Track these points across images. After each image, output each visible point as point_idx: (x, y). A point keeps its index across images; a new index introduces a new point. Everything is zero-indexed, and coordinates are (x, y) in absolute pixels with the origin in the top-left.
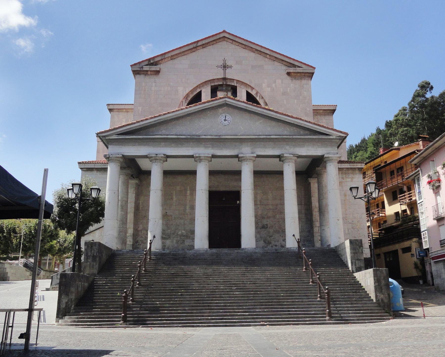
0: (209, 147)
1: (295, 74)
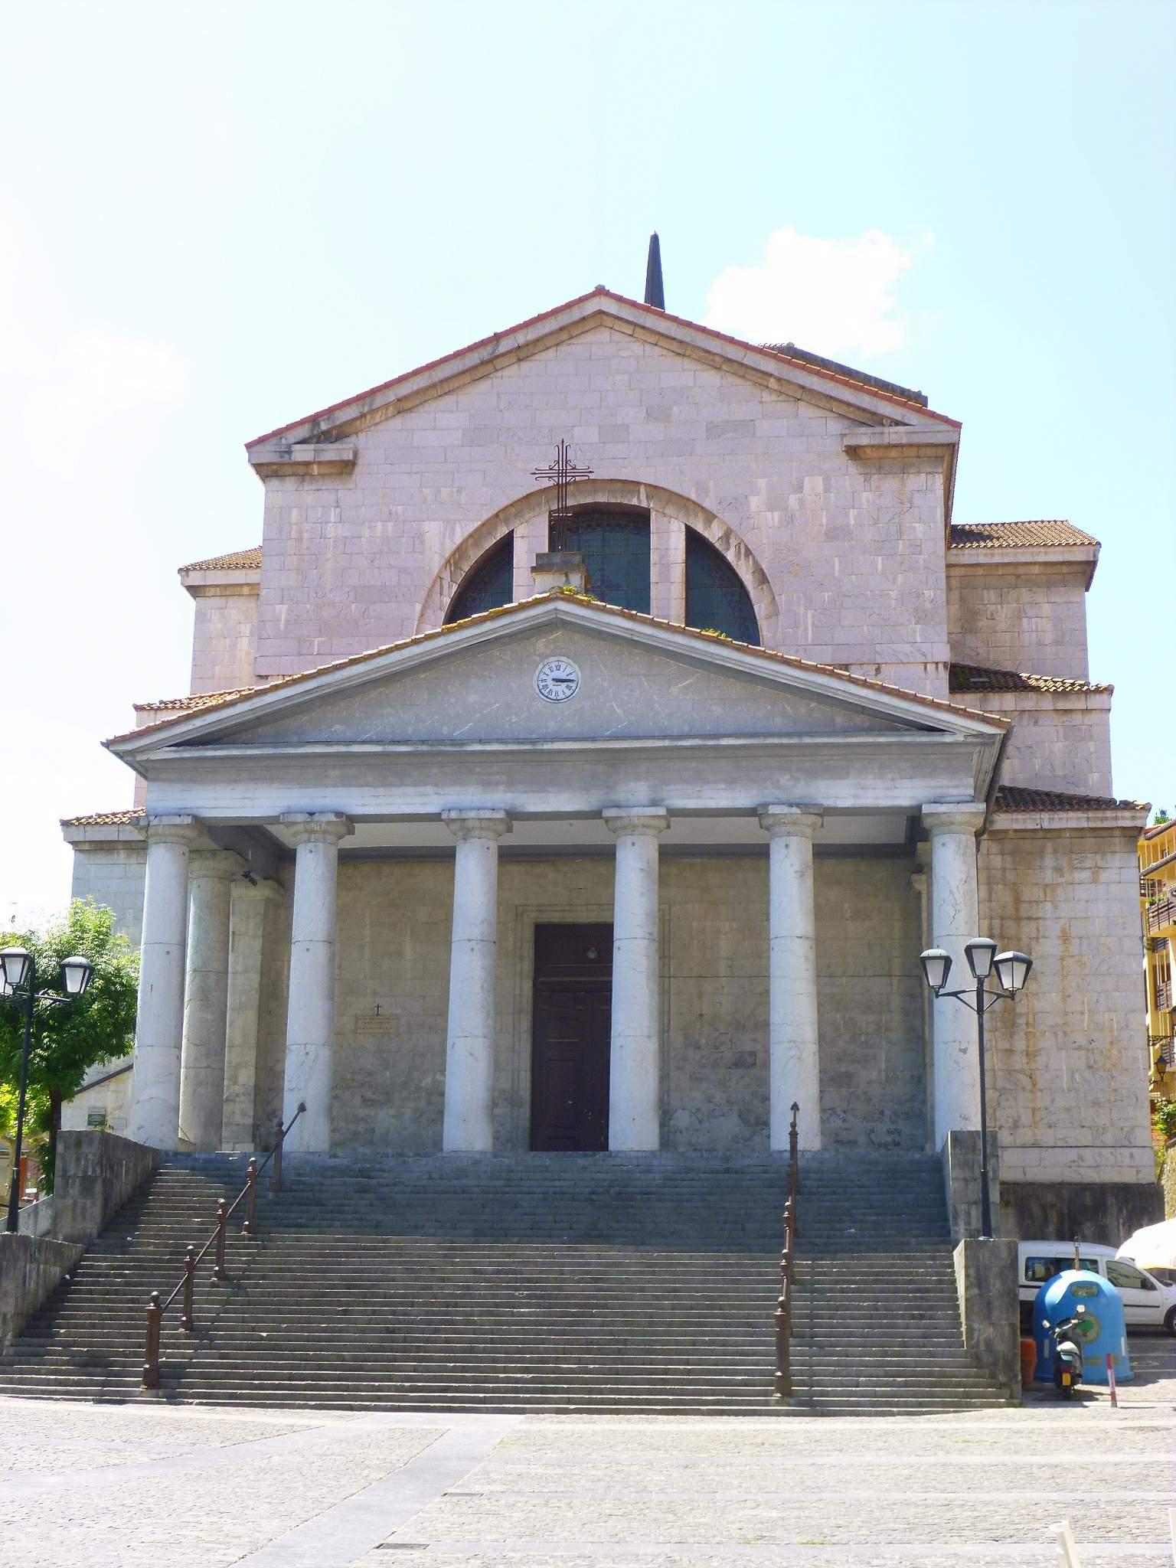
0: (497, 783)
1: (880, 453)
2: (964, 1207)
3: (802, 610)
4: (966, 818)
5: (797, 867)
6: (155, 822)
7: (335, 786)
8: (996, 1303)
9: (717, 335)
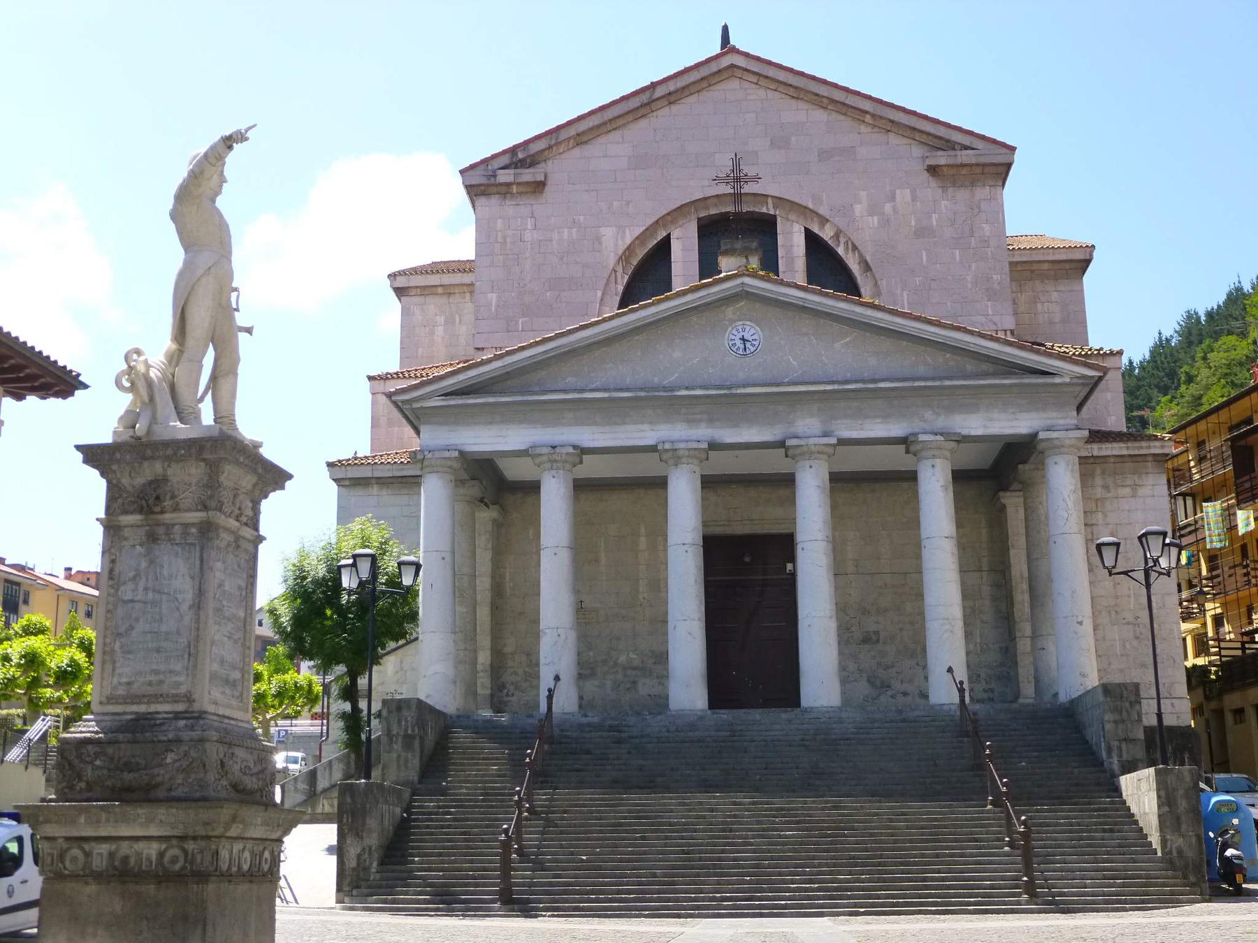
0: (700, 421)
2: (1116, 743)
3: (899, 292)
4: (1073, 442)
5: (942, 483)
6: (430, 456)
7: (570, 425)
8: (1183, 818)
9: (825, 82)
